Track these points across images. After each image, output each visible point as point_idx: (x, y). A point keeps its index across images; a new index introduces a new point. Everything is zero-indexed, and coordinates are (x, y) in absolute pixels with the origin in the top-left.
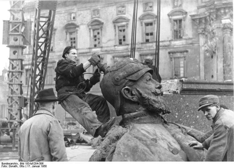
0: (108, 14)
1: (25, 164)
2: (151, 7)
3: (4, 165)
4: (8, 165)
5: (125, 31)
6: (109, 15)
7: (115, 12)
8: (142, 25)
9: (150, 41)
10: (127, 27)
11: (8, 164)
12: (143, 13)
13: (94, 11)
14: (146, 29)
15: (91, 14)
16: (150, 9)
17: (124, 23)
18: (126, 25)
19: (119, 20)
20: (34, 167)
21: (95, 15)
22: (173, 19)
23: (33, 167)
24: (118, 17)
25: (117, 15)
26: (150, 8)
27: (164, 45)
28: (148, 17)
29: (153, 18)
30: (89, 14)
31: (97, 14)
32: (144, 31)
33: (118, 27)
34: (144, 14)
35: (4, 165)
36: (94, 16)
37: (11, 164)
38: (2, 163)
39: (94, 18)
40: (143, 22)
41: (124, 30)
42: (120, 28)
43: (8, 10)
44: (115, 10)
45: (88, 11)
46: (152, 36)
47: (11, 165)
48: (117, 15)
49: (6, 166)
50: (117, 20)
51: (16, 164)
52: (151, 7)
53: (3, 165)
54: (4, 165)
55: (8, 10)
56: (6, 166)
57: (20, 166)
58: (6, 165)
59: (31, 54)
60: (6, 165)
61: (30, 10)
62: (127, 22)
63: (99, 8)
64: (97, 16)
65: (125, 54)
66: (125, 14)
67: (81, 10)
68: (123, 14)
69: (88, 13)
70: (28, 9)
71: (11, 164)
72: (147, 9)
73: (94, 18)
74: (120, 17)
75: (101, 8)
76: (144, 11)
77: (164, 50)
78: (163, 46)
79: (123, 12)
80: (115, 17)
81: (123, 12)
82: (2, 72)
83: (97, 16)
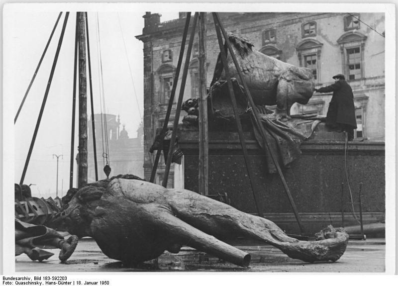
0: (289, 36)
1: (42, 278)
2: (356, 22)
3: (6, 281)
4: (14, 281)
5: (317, 63)
6: (291, 38)
7: (168, 47)
8: (343, 53)
9: (355, 78)
10: (319, 56)
11: (14, 279)
12: (344, 33)
13: (267, 32)
14: (348, 59)
15: (263, 38)
16: (355, 25)
17: (314, 51)
18: (317, 54)
19: (307, 46)
20: (50, 283)
21: (269, 39)
22: (345, 48)
23: (86, 285)
24: (305, 40)
25: (304, 37)
26: (354, 24)
27: (377, 83)
28: (352, 38)
29: (361, 41)
30: (259, 38)
31: (272, 37)
32: (346, 63)
33: (305, 57)
34: (344, 35)
35: (6, 281)
36: (267, 41)
37: (19, 279)
38: (4, 278)
39: (268, 43)
40: (343, 47)
41: (314, 62)
42: (309, 59)
43: (137, 37)
44: (299, 29)
45: (258, 33)
46: (359, 70)
47: (19, 281)
48: (304, 37)
49: (11, 283)
50: (303, 45)
51: (27, 279)
52: (356, 22)
53: (5, 280)
54: (7, 281)
55: (137, 37)
56: (11, 283)
57: (17, 283)
58: (9, 281)
59: (166, 105)
60: (9, 281)
61: (169, 36)
62: (320, 49)
63: (275, 28)
64: (272, 40)
65: (316, 100)
66: (315, 35)
67: (246, 33)
68: (312, 36)
69: (256, 37)
70: (166, 34)
71: (19, 279)
72: (351, 26)
73: (268, 43)
74: (308, 41)
75: (276, 27)
76: (346, 30)
77: (378, 92)
78: (376, 86)
79: (312, 33)
80: (300, 40)
81: (312, 32)
82: (137, 133)
83: (272, 40)
